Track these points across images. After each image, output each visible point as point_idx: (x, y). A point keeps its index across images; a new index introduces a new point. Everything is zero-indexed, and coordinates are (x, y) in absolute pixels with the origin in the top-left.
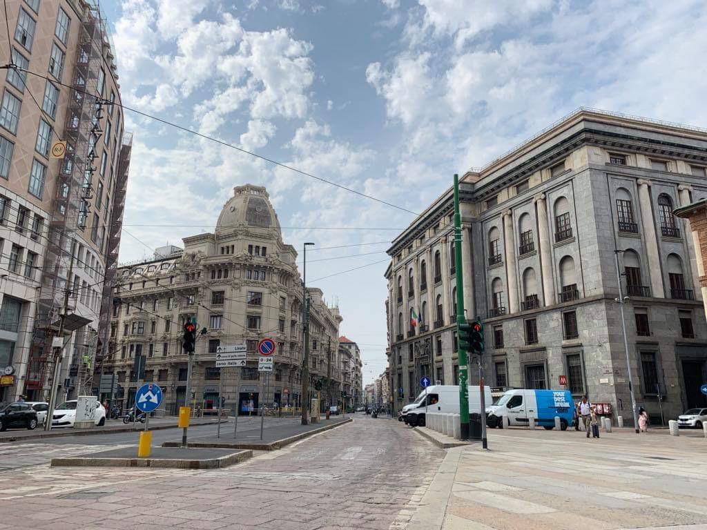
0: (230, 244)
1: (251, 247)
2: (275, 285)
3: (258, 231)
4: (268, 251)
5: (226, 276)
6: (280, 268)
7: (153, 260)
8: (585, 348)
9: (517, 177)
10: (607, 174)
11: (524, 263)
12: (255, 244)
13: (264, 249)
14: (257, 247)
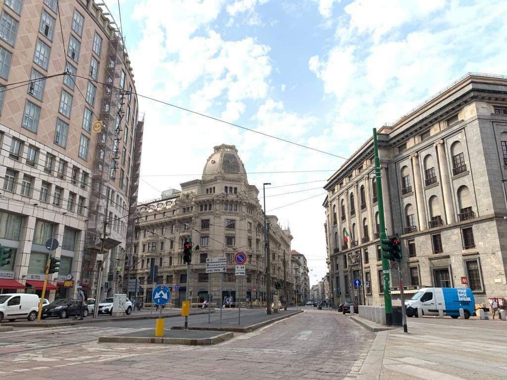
0: (212, 186)
1: (226, 188)
2: (244, 214)
3: (231, 176)
4: (238, 190)
5: (210, 209)
6: (247, 201)
7: (161, 199)
8: (481, 256)
9: (421, 128)
10: (493, 122)
11: (429, 193)
12: (229, 186)
13: (236, 189)
14: (231, 188)
